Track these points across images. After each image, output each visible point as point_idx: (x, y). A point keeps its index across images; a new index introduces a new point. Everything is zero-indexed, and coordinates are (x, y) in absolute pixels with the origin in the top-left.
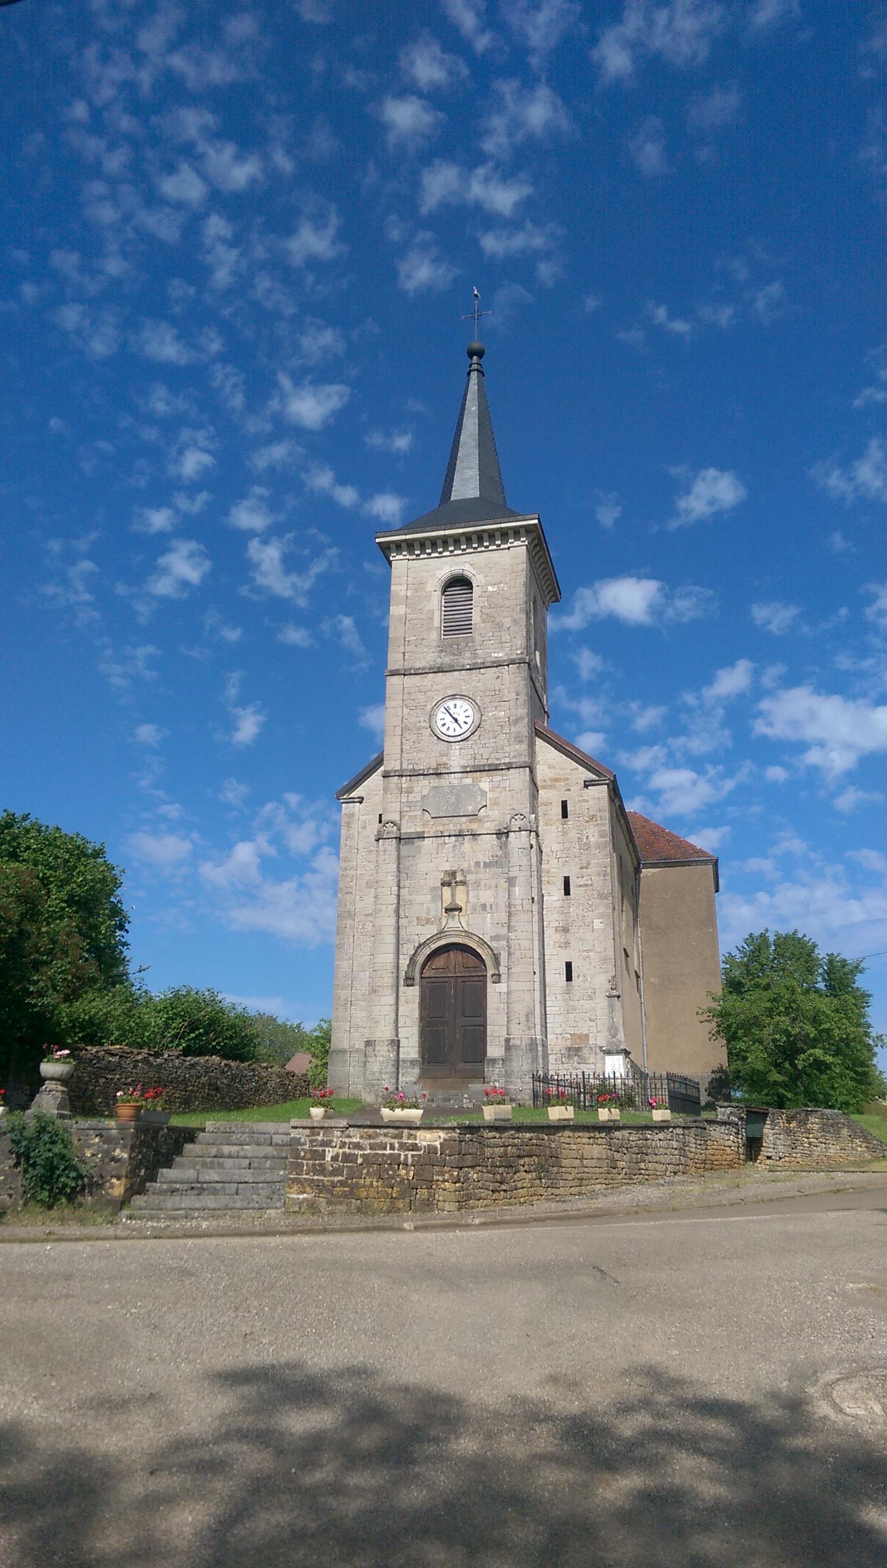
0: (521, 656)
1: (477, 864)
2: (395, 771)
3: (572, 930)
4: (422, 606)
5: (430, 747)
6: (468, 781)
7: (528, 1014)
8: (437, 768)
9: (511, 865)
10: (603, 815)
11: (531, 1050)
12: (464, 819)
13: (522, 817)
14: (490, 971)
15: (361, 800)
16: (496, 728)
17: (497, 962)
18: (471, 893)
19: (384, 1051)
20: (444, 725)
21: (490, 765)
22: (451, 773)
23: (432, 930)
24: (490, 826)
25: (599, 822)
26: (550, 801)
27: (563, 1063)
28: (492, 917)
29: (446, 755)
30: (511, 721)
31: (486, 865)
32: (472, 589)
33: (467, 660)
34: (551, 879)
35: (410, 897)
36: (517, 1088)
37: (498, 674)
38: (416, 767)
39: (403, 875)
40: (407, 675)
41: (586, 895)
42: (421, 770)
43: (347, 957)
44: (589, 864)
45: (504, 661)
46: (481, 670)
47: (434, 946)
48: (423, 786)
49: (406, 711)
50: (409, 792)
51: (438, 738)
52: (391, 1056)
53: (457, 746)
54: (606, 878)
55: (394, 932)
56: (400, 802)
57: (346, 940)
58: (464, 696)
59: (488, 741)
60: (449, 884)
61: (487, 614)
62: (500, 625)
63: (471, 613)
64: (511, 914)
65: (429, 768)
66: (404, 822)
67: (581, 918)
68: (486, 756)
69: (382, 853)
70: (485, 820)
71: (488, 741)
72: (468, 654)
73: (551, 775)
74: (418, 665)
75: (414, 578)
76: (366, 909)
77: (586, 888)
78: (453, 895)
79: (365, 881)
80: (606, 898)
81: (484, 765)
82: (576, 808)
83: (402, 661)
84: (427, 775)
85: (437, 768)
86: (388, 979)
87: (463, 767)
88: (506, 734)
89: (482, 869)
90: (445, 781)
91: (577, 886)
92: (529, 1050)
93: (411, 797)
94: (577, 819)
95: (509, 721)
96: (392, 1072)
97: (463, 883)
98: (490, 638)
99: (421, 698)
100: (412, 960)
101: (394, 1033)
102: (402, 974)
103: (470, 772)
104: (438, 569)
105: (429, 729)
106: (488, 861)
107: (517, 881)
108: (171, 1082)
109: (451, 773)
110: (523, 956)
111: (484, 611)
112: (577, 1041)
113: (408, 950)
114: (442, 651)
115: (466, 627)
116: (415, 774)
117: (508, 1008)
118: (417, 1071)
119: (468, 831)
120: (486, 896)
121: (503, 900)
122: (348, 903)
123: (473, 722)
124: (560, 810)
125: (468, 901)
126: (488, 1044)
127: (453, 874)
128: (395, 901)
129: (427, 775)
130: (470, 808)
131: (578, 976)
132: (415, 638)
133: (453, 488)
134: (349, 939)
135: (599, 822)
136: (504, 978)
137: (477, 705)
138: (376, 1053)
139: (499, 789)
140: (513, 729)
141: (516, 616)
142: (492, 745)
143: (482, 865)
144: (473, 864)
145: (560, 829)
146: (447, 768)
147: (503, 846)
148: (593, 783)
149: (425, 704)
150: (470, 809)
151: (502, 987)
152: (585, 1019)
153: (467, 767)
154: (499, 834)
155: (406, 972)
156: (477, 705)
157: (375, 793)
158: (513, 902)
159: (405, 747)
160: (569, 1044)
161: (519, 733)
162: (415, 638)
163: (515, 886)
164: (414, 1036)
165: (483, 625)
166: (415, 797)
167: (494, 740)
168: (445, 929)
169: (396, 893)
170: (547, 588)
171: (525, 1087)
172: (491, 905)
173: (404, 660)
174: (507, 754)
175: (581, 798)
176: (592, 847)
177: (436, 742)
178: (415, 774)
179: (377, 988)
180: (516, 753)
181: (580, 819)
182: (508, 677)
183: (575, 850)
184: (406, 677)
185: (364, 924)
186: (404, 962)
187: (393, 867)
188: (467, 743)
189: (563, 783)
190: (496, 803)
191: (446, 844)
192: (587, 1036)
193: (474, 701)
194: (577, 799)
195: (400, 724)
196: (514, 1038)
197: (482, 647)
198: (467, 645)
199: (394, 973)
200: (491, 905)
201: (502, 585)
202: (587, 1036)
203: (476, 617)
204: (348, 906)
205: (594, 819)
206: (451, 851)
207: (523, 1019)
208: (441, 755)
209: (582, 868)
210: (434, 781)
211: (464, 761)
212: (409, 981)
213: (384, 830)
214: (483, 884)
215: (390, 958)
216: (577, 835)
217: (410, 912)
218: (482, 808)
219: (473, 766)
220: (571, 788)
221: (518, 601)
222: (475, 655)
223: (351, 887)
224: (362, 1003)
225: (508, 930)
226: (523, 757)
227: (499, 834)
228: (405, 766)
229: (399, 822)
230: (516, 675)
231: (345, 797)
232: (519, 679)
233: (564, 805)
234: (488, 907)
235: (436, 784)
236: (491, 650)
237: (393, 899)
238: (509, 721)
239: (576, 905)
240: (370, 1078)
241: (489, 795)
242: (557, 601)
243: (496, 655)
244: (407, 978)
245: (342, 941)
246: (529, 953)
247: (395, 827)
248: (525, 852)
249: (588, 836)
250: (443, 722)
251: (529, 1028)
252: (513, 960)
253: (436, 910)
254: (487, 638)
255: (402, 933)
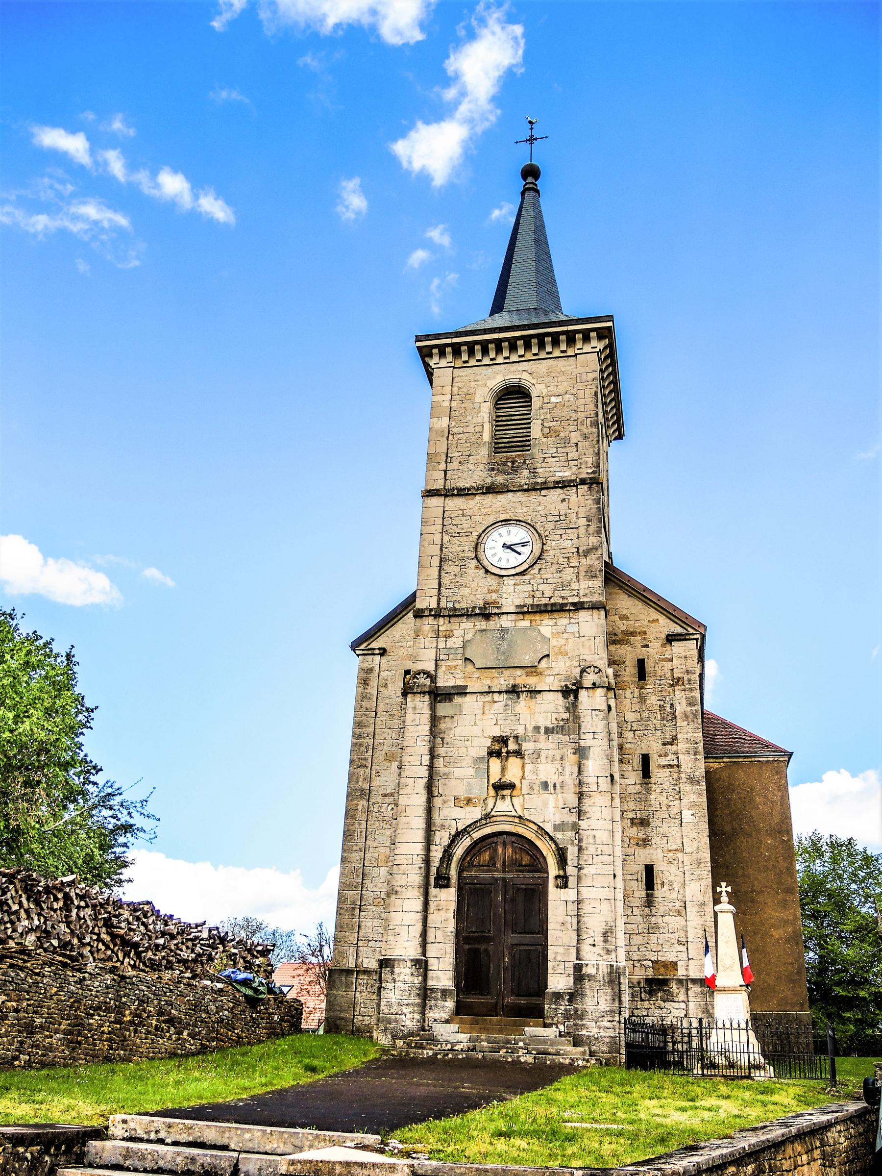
0: (593, 475)
1: (537, 728)
2: (431, 610)
3: (654, 823)
4: (469, 418)
5: (476, 582)
6: (525, 623)
7: (606, 932)
8: (485, 607)
9: (582, 731)
10: (692, 678)
11: (611, 982)
12: (519, 672)
13: (596, 670)
14: (553, 870)
15: (383, 652)
16: (561, 560)
17: (562, 860)
18: (528, 767)
19: (405, 974)
20: (495, 554)
21: (553, 605)
22: (503, 614)
23: (474, 813)
24: (551, 682)
25: (687, 686)
26: (623, 659)
27: (642, 1000)
28: (557, 800)
29: (496, 592)
30: (580, 551)
31: (548, 731)
32: (530, 402)
33: (523, 478)
34: (625, 756)
35: (446, 770)
36: (591, 1034)
37: (563, 496)
38: (457, 606)
39: (438, 741)
40: (448, 496)
41: (671, 778)
42: (464, 609)
43: (357, 848)
44: (675, 738)
45: (571, 481)
46: (542, 492)
47: (477, 835)
48: (465, 629)
49: (446, 538)
50: (447, 637)
51: (487, 571)
52: (416, 981)
53: (510, 581)
54: (698, 757)
55: (424, 815)
56: (437, 648)
57: (356, 826)
58: (520, 521)
59: (551, 576)
60: (498, 754)
61: (549, 428)
62: (566, 441)
63: (529, 428)
64: (582, 795)
65: (475, 607)
66: (440, 673)
67: (664, 808)
68: (547, 593)
69: (410, 711)
70: (547, 672)
71: (551, 576)
72: (526, 473)
73: (623, 628)
74: (462, 484)
75: (459, 388)
76: (383, 787)
77: (671, 770)
78: (503, 769)
79: (383, 752)
80: (698, 783)
81: (546, 605)
82: (657, 668)
83: (443, 481)
84: (471, 615)
85: (485, 607)
86: (416, 878)
87: (517, 606)
88: (573, 567)
89: (542, 737)
90: (494, 624)
91: (659, 766)
92: (608, 983)
93: (450, 643)
94: (658, 682)
95: (578, 552)
96: (417, 1005)
97: (518, 753)
98: (554, 455)
99: (466, 524)
100: (447, 854)
101: (420, 950)
102: (434, 870)
103: (528, 612)
104: (490, 378)
105: (475, 560)
106: (551, 726)
107: (591, 753)
108: (99, 1008)
109: (503, 614)
110: (599, 853)
111: (546, 424)
112: (662, 970)
113: (442, 838)
114: (493, 469)
115: (525, 444)
116: (456, 614)
117: (578, 922)
118: (450, 1004)
119: (525, 687)
120: (547, 771)
121: (570, 780)
122: (361, 779)
123: (532, 551)
124: (635, 671)
125: (523, 777)
126: (550, 971)
127: (504, 741)
128: (426, 774)
129: (471, 615)
130: (527, 657)
131: (663, 884)
132: (460, 454)
133: (511, 280)
134: (360, 824)
135: (687, 686)
136: (572, 881)
137: (537, 532)
138: (395, 976)
139: (565, 636)
140: (583, 561)
141: (586, 431)
142: (555, 581)
143: (542, 731)
144: (530, 728)
145: (636, 694)
146: (498, 608)
147: (573, 708)
148: (679, 638)
149: (470, 530)
150: (527, 659)
151: (570, 894)
152: (673, 941)
153: (525, 606)
154: (566, 692)
155: (438, 868)
156: (537, 532)
157: (400, 644)
158: (585, 780)
159: (443, 582)
160: (650, 973)
161: (591, 566)
162: (460, 454)
163: (587, 759)
164: (448, 956)
165: (544, 440)
166: (455, 642)
167: (559, 575)
168: (493, 813)
169: (428, 763)
170: (612, 417)
171: (603, 1034)
172: (555, 784)
173: (446, 479)
174: (575, 593)
175: (662, 657)
176: (678, 717)
177: (484, 576)
178: (456, 614)
179: (398, 889)
180: (588, 591)
181: (662, 682)
182: (576, 499)
183: (655, 722)
184: (447, 499)
185: (381, 807)
186: (437, 854)
187: (425, 729)
188: (524, 577)
189: (638, 638)
190: (562, 653)
191: (495, 702)
192: (675, 964)
193: (533, 527)
194: (657, 657)
195: (439, 552)
196: (587, 965)
197: (543, 465)
198: (524, 462)
199: (423, 869)
200: (555, 784)
201: (568, 396)
202: (675, 964)
203: (536, 431)
204: (360, 783)
205: (680, 683)
206: (501, 711)
207: (599, 939)
208: (490, 592)
209: (664, 744)
210: (482, 624)
211: (519, 600)
212: (442, 881)
213: (415, 683)
214: (543, 755)
215: (418, 849)
216: (659, 703)
217: (448, 788)
218: (542, 658)
219: (532, 606)
220: (650, 644)
221: (588, 413)
222: (534, 473)
223: (365, 759)
224: (374, 908)
225: (579, 817)
226: (597, 595)
227: (566, 692)
228: (443, 604)
229: (433, 673)
230: (587, 497)
231: (362, 647)
232: (590, 502)
233: (641, 663)
234: (551, 787)
235: (484, 627)
236: (554, 469)
237: (424, 772)
238: (578, 552)
239: (658, 790)
240: (386, 1011)
241: (553, 642)
242: (620, 437)
243: (561, 474)
244: (439, 877)
245: (351, 828)
246: (607, 850)
247: (429, 680)
248: (602, 715)
249: (672, 704)
250: (492, 552)
251: (608, 952)
252: (585, 857)
253: (480, 789)
254: (550, 455)
255: (435, 815)
